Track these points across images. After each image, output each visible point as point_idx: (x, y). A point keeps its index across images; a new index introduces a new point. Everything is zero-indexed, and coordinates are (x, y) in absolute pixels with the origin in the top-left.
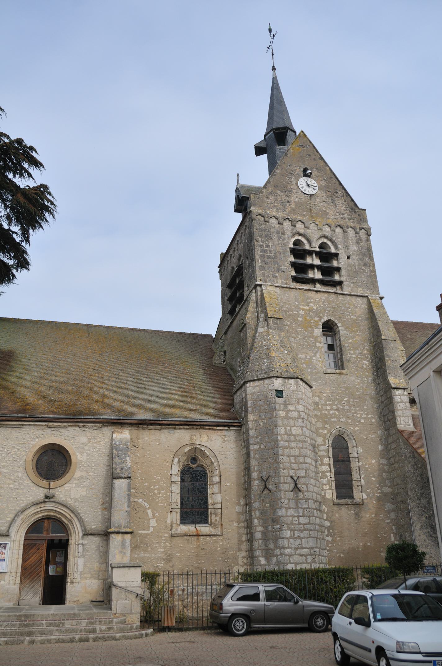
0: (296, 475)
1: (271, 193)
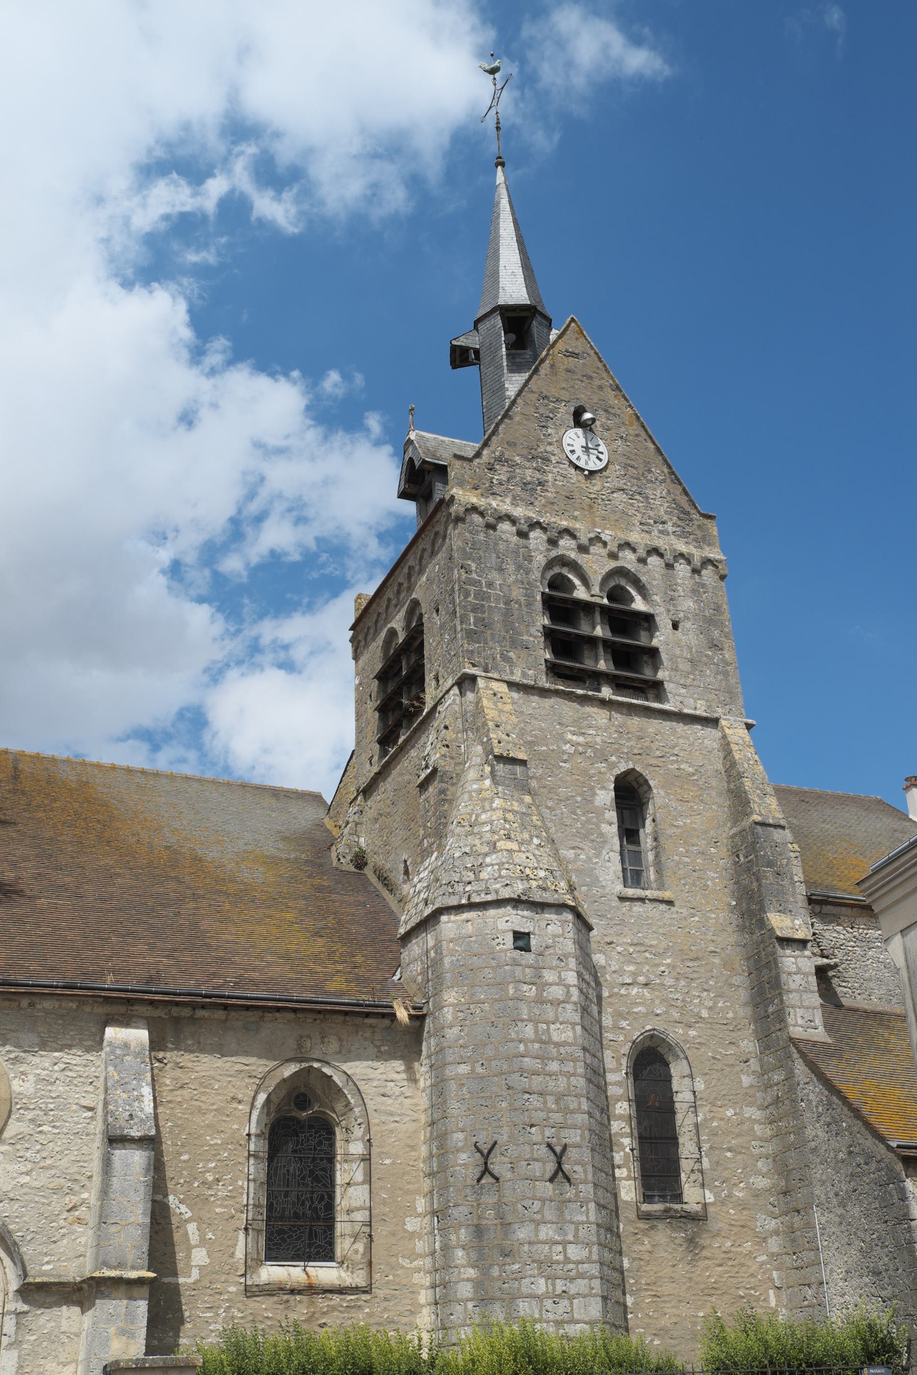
0: (559, 1139)
1: (499, 460)
